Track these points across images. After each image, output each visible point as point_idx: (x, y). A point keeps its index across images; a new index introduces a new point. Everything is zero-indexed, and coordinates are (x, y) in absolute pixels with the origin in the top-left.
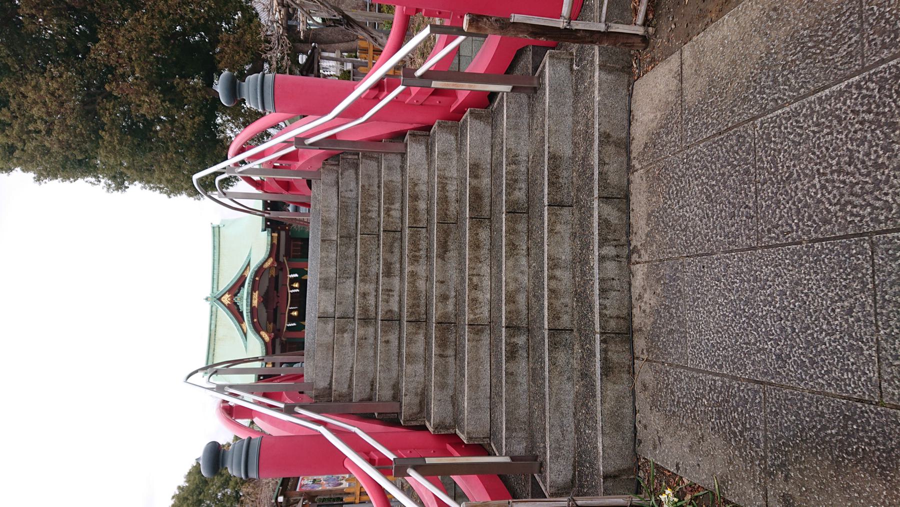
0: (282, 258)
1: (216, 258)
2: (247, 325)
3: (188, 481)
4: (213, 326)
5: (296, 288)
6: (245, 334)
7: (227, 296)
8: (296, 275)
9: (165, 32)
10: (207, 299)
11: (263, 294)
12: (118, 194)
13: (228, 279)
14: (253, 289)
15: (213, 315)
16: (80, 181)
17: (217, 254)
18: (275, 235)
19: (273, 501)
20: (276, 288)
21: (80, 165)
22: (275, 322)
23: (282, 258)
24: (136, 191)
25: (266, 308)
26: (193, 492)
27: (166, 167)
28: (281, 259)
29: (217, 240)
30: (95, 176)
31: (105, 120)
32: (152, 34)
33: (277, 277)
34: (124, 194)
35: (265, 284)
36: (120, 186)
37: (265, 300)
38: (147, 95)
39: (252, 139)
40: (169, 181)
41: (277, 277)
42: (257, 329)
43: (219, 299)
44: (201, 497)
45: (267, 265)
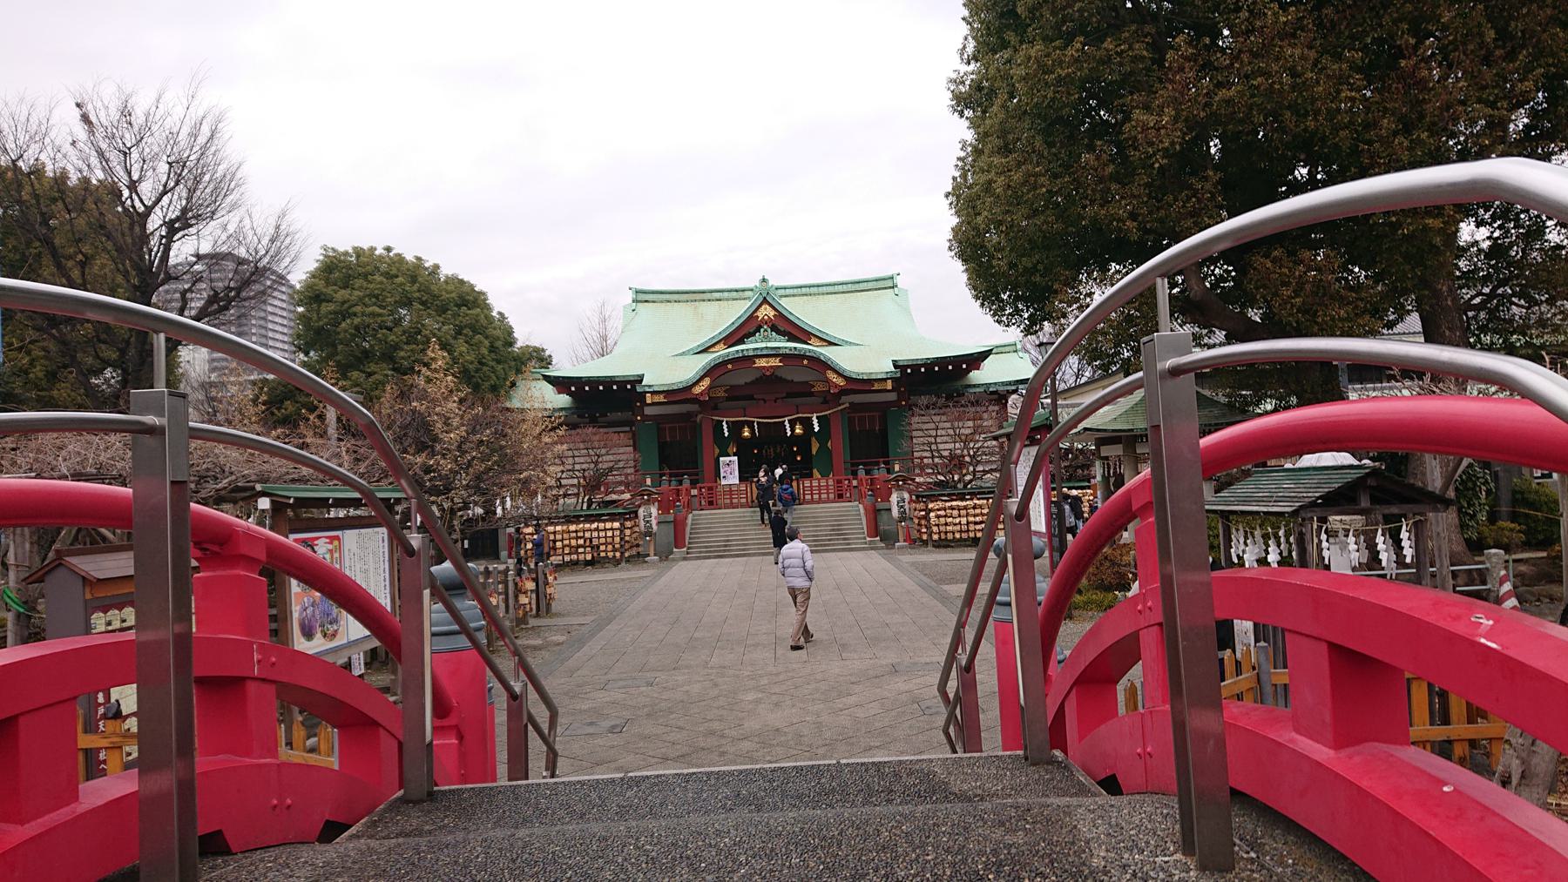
0: (846, 401)
1: (837, 288)
2: (722, 352)
3: (449, 280)
4: (717, 295)
5: (793, 430)
6: (705, 351)
7: (772, 314)
8: (817, 429)
9: (1323, 139)
10: (764, 280)
11: (778, 373)
12: (946, 99)
13: (802, 311)
14: (786, 357)
15: (738, 293)
16: (964, 29)
17: (845, 288)
18: (889, 385)
19: (259, 487)
20: (789, 395)
21: (1002, 15)
22: (728, 399)
23: (846, 401)
24: (956, 134)
25: (752, 383)
26: (427, 290)
27: (1017, 177)
28: (844, 398)
29: (870, 285)
30: (977, 50)
31: (1108, 44)
32: (1317, 113)
33: (812, 394)
34: (947, 112)
35: (797, 375)
36: (962, 102)
37: (769, 380)
38: (1176, 120)
39: (1391, 378)
40: (988, 187)
41: (812, 394)
42: (712, 371)
43: (765, 301)
44: (416, 305)
45: (831, 375)
